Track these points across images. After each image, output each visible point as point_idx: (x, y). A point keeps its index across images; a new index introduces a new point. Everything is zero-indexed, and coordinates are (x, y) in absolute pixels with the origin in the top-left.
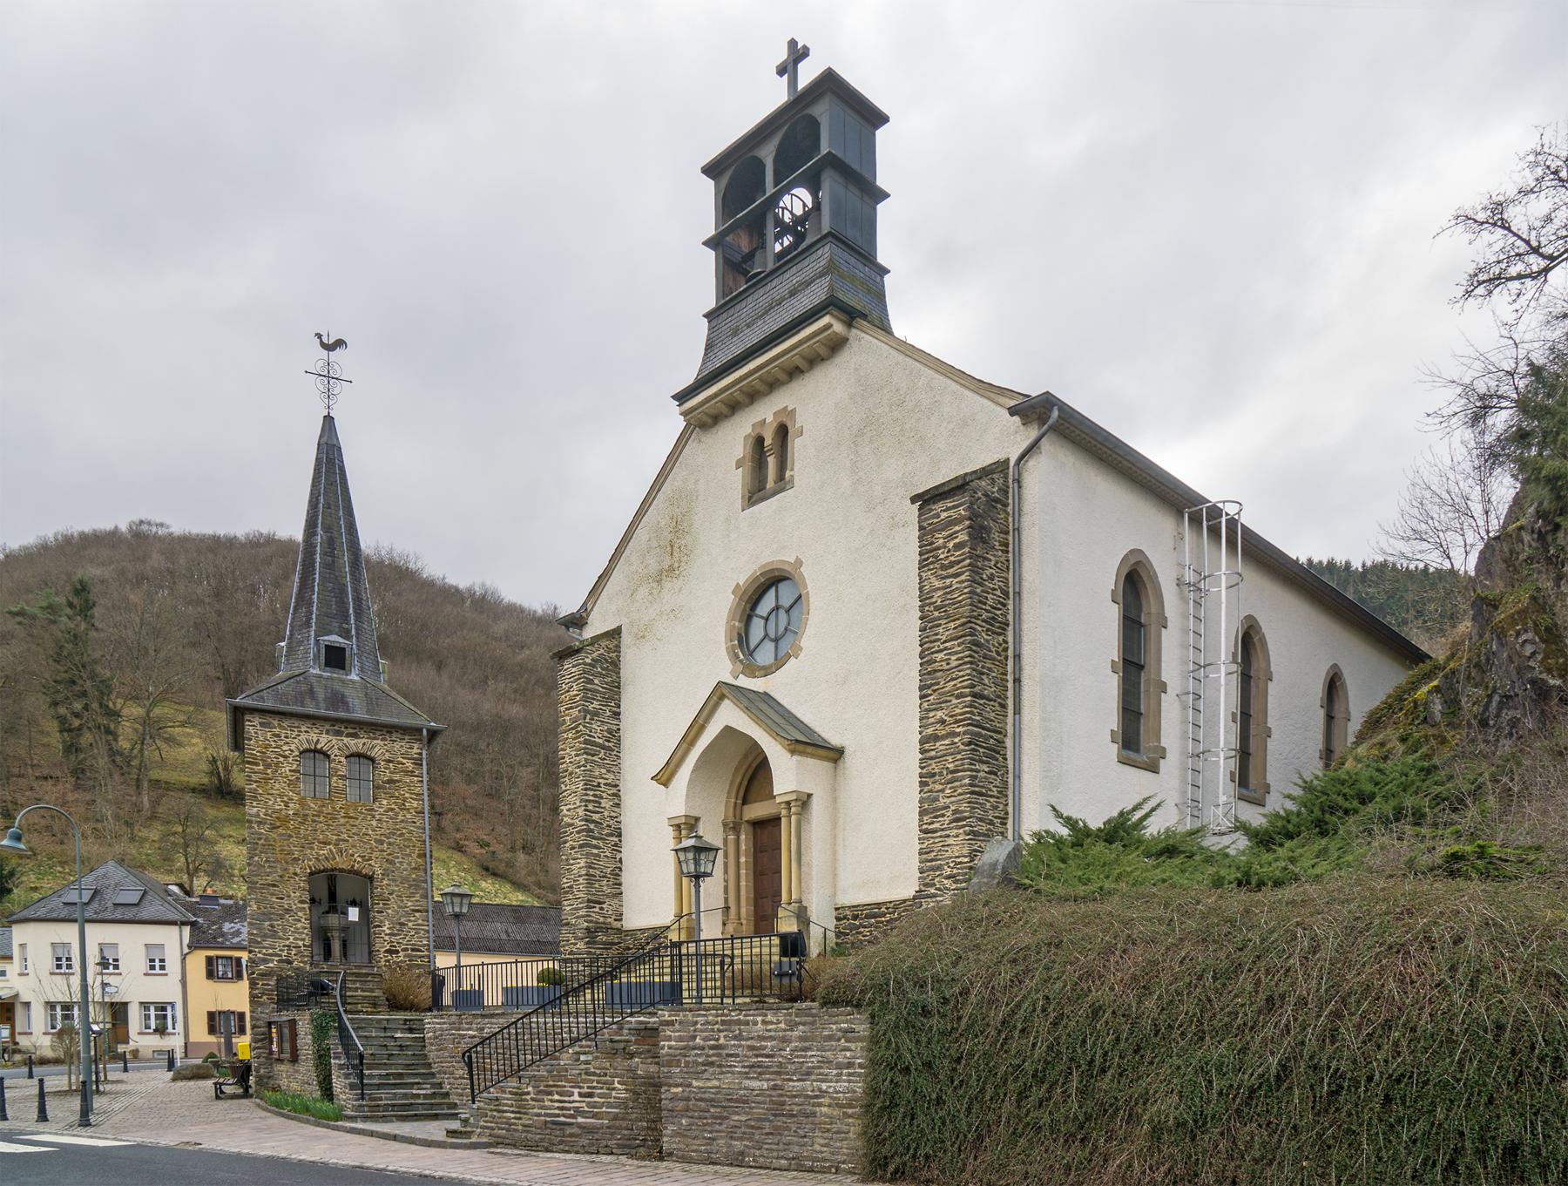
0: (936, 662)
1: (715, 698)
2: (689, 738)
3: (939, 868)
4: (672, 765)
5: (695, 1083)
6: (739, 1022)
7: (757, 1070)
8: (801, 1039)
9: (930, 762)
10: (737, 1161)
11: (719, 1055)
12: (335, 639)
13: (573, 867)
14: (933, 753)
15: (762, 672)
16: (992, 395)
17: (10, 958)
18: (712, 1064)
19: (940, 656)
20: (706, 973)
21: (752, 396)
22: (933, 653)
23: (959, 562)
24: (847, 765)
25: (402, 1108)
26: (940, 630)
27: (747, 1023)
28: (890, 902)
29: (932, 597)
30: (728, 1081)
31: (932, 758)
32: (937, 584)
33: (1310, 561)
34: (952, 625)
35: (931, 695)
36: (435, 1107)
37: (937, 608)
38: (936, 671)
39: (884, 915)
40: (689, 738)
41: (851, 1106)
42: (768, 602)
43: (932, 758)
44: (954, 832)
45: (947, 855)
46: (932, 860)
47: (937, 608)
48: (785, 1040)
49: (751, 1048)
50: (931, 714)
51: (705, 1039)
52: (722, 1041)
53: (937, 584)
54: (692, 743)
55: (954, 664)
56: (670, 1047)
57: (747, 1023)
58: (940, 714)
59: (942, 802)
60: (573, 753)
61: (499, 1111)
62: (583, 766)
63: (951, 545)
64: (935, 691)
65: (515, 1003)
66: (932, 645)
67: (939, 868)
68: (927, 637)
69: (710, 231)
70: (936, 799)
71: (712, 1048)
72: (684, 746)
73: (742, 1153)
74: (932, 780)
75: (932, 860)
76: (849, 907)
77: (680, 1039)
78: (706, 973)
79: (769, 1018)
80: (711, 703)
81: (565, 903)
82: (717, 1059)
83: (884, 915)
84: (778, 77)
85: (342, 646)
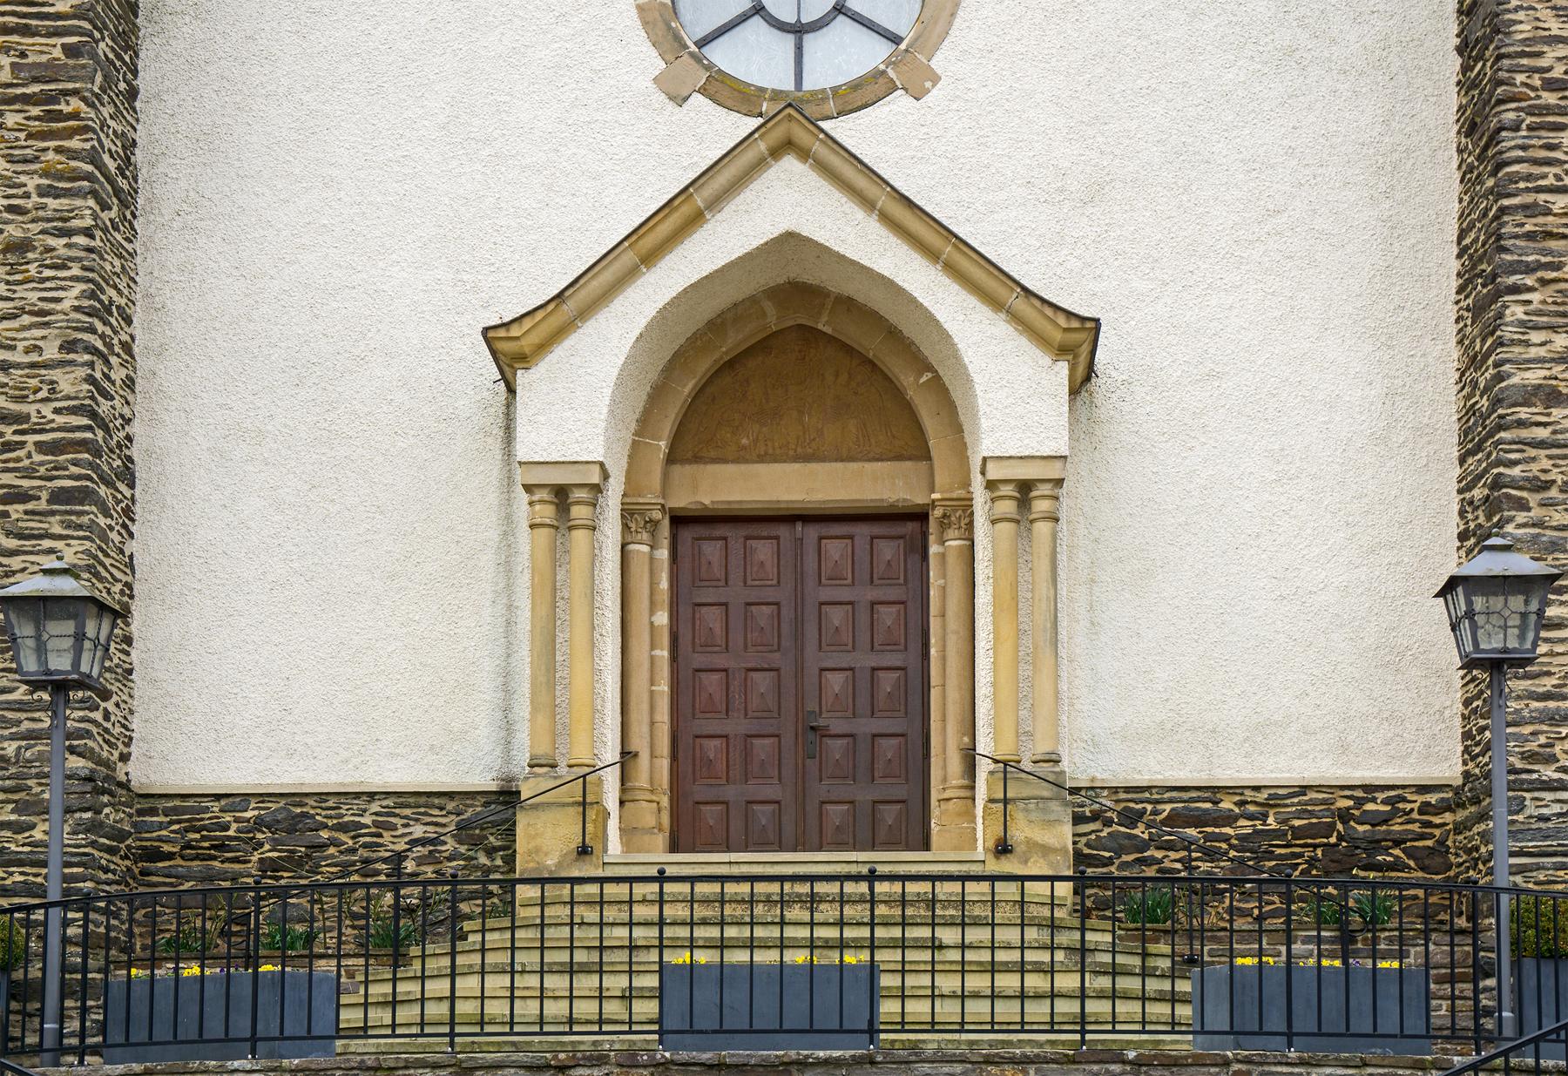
0: (1548, 212)
1: (763, 146)
2: (649, 241)
4: (570, 307)
9: (1532, 452)
17: (674, 847)
22: (1539, 190)
24: (1103, 412)
28: (1257, 788)
29: (1539, 54)
31: (1541, 444)
35: (1531, 289)
38: (1550, 235)
39: (1230, 819)
40: (649, 241)
43: (1541, 444)
46: (1547, 696)
50: (1536, 337)
54: (650, 259)
60: (32, 183)
62: (88, 233)
64: (1544, 282)
66: (1536, 170)
68: (1524, 148)
72: (628, 258)
74: (1538, 496)
75: (1547, 696)
76: (1115, 790)
80: (749, 156)
83: (1230, 819)
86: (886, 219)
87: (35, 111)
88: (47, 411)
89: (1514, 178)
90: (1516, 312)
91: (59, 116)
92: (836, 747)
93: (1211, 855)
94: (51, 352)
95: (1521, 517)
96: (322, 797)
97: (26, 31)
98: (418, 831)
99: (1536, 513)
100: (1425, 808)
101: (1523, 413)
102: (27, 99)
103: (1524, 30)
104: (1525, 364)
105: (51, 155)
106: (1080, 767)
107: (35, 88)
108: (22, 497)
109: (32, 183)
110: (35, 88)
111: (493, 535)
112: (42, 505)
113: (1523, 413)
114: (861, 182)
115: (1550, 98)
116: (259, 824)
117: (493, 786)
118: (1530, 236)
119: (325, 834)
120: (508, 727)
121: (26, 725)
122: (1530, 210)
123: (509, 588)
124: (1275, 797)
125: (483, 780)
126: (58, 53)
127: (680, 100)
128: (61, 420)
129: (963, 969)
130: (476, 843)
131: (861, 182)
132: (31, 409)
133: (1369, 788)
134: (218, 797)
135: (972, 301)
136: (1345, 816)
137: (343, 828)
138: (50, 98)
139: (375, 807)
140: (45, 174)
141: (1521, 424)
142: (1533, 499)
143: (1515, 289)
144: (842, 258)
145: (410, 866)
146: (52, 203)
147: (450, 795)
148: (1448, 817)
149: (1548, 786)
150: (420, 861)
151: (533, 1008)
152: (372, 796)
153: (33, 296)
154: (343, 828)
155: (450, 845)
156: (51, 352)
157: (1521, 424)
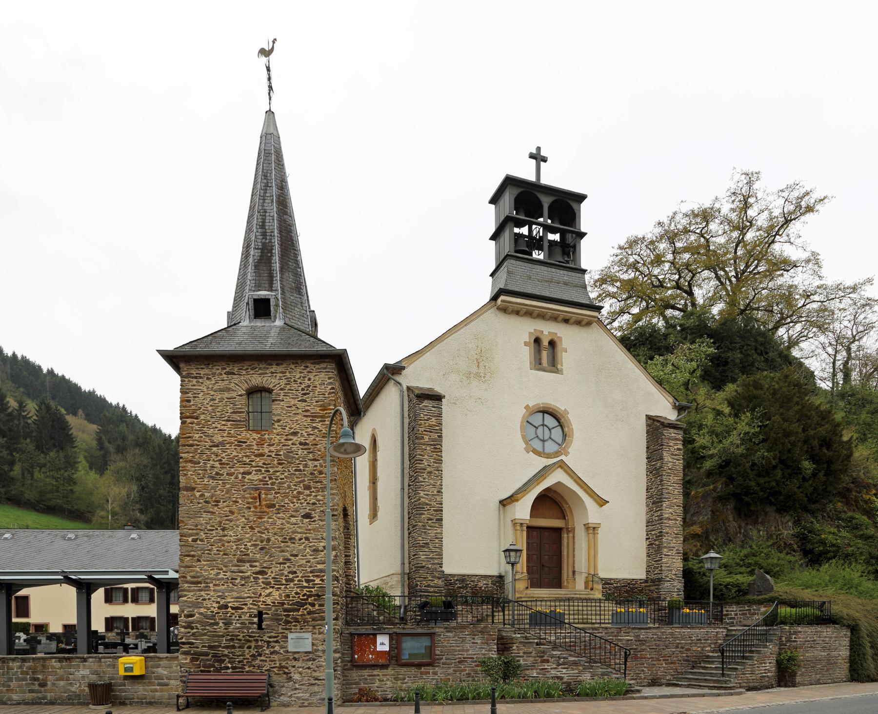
3: (671, 570)
5: (807, 655)
6: (820, 632)
7: (824, 649)
8: (836, 637)
10: (818, 682)
11: (814, 644)
12: (263, 293)
13: (430, 532)
14: (668, 525)
15: (546, 456)
16: (453, 332)
18: (811, 647)
19: (671, 488)
20: (578, 606)
21: (554, 318)
23: (678, 455)
25: (695, 680)
26: (671, 478)
27: (822, 632)
30: (816, 653)
31: (668, 527)
32: (670, 460)
33: (14, 355)
34: (676, 478)
36: (691, 680)
37: (669, 469)
39: (612, 584)
41: (845, 659)
42: (550, 421)
43: (668, 527)
44: (677, 557)
45: (674, 566)
47: (669, 469)
48: (831, 638)
49: (823, 641)
50: (667, 509)
51: (810, 638)
52: (815, 638)
53: (670, 460)
55: (675, 493)
56: (800, 641)
57: (822, 632)
58: (670, 510)
59: (672, 545)
60: (432, 461)
61: (743, 674)
63: (676, 447)
65: (700, 622)
67: (671, 570)
69: (584, 242)
70: (670, 543)
71: (812, 641)
73: (819, 679)
77: (804, 638)
78: (578, 606)
79: (828, 630)
81: (421, 553)
82: (813, 645)
83: (612, 584)
84: (528, 156)
85: (267, 297)
86: (575, 481)
87: (432, 447)
88: (435, 503)
89: (665, 483)
90: (664, 505)
91: (436, 448)
92: (547, 569)
93: (610, 590)
94: (435, 493)
95: (665, 538)
96: (468, 575)
97: (431, 432)
98: (485, 582)
99: (667, 537)
100: (640, 583)
101: (665, 521)
102: (431, 445)
103: (666, 460)
104: (666, 513)
105: (435, 456)
106: (602, 575)
107: (432, 443)
108: (431, 519)
109: (432, 461)
110: (432, 443)
111: (497, 529)
112: (434, 521)
113: (665, 521)
114: (572, 474)
115: (669, 471)
116: (457, 580)
117: (498, 575)
118: (667, 493)
119: (468, 582)
120: (500, 564)
121: (432, 562)
122: (667, 489)
123: (500, 539)
124: (619, 581)
125: (495, 573)
126: (436, 437)
127: (528, 452)
128: (437, 505)
129: (596, 606)
130: (495, 585)
131: (572, 474)
132: (432, 503)
133: (633, 579)
134: (450, 575)
135: (588, 496)
136: (629, 584)
137: (471, 581)
138: (435, 445)
139: (477, 578)
140: (434, 459)
141: (665, 523)
142: (666, 535)
143: (664, 501)
144: (567, 486)
145: (483, 588)
146: (435, 465)
147: (490, 576)
148: (643, 584)
149: (668, 581)
150: (485, 588)
151: (586, 612)
152: (477, 576)
153: (432, 482)
154: (471, 581)
155: (490, 585)
156: (435, 493)
157: (665, 523)
